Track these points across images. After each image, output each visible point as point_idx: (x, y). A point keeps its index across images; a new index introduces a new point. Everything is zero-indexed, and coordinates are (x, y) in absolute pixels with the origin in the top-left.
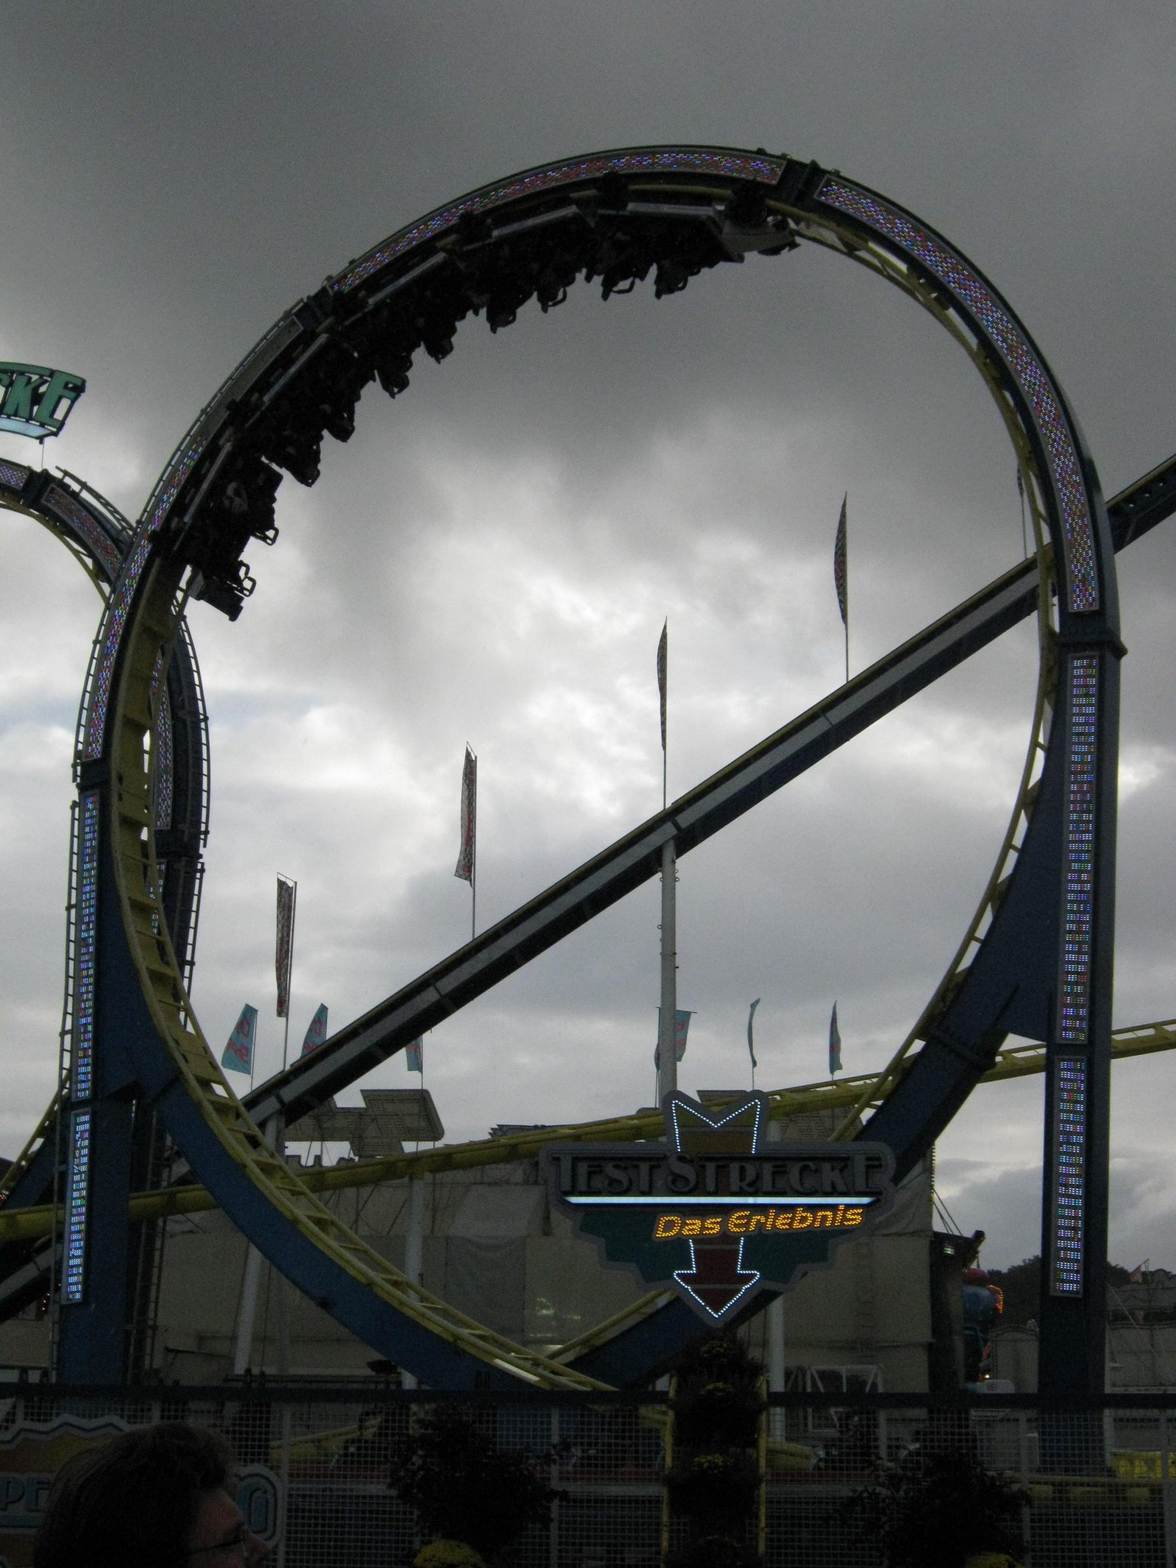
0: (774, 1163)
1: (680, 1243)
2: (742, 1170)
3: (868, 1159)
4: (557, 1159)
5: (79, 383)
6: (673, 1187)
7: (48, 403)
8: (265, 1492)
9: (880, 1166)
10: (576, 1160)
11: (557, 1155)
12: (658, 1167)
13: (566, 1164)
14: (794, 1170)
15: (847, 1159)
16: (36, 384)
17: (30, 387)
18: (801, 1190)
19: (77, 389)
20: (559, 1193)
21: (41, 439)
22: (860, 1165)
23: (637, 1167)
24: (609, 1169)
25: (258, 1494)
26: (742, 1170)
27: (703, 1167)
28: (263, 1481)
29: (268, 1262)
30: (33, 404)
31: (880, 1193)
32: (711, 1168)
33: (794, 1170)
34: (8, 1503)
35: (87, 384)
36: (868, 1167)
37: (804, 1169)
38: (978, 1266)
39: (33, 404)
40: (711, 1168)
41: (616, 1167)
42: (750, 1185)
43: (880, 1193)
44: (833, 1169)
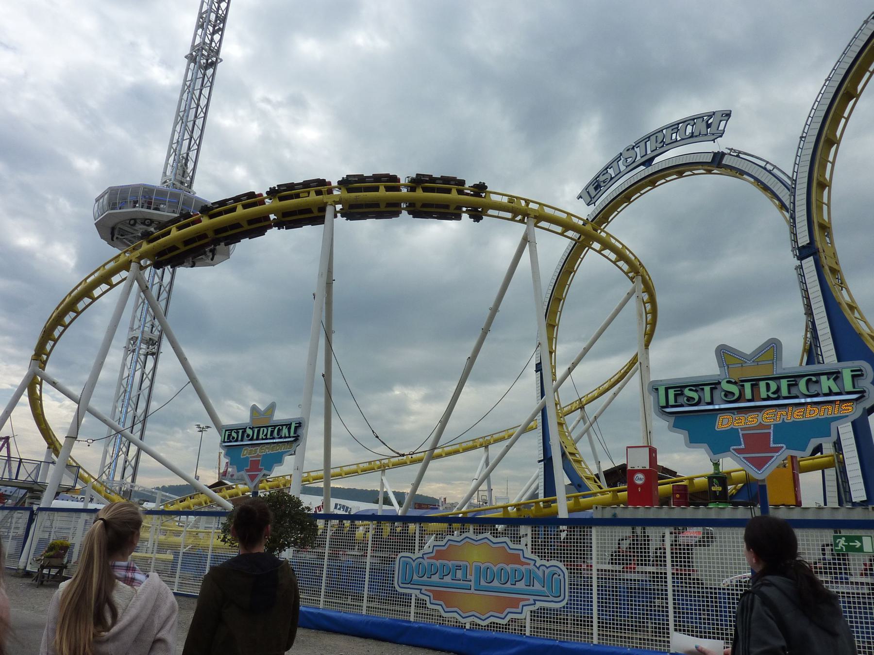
0: (787, 380)
1: (734, 431)
2: (768, 386)
3: (852, 371)
4: (657, 389)
5: (729, 112)
6: (726, 399)
7: (714, 126)
8: (559, 575)
9: (862, 375)
10: (667, 389)
11: (657, 387)
12: (716, 388)
13: (662, 392)
14: (802, 383)
15: (838, 372)
16: (707, 120)
17: (705, 122)
18: (807, 393)
19: (728, 115)
20: (660, 408)
21: (714, 140)
22: (847, 376)
23: (703, 389)
24: (687, 392)
25: (556, 576)
26: (768, 386)
27: (743, 386)
28: (556, 569)
29: (110, 428)
30: (707, 128)
31: (864, 392)
32: (748, 386)
33: (802, 383)
34: (516, 581)
35: (732, 113)
36: (853, 377)
37: (808, 382)
38: (153, 357)
39: (707, 128)
40: (748, 386)
41: (690, 390)
42: (773, 393)
43: (864, 392)
44: (828, 379)
